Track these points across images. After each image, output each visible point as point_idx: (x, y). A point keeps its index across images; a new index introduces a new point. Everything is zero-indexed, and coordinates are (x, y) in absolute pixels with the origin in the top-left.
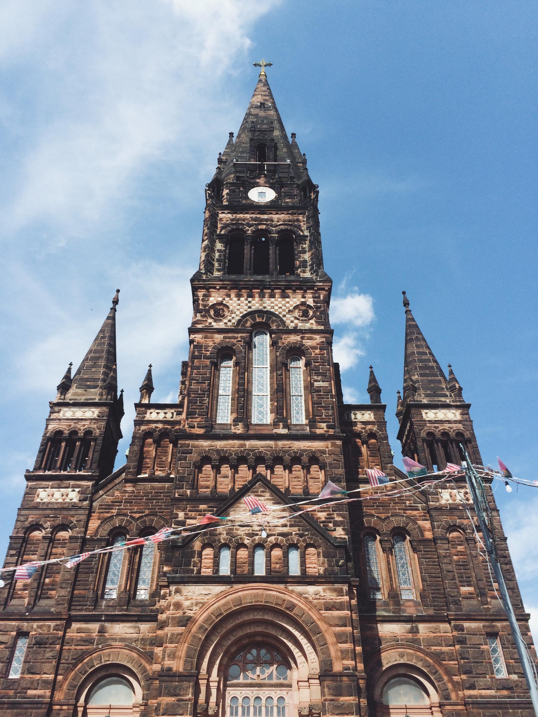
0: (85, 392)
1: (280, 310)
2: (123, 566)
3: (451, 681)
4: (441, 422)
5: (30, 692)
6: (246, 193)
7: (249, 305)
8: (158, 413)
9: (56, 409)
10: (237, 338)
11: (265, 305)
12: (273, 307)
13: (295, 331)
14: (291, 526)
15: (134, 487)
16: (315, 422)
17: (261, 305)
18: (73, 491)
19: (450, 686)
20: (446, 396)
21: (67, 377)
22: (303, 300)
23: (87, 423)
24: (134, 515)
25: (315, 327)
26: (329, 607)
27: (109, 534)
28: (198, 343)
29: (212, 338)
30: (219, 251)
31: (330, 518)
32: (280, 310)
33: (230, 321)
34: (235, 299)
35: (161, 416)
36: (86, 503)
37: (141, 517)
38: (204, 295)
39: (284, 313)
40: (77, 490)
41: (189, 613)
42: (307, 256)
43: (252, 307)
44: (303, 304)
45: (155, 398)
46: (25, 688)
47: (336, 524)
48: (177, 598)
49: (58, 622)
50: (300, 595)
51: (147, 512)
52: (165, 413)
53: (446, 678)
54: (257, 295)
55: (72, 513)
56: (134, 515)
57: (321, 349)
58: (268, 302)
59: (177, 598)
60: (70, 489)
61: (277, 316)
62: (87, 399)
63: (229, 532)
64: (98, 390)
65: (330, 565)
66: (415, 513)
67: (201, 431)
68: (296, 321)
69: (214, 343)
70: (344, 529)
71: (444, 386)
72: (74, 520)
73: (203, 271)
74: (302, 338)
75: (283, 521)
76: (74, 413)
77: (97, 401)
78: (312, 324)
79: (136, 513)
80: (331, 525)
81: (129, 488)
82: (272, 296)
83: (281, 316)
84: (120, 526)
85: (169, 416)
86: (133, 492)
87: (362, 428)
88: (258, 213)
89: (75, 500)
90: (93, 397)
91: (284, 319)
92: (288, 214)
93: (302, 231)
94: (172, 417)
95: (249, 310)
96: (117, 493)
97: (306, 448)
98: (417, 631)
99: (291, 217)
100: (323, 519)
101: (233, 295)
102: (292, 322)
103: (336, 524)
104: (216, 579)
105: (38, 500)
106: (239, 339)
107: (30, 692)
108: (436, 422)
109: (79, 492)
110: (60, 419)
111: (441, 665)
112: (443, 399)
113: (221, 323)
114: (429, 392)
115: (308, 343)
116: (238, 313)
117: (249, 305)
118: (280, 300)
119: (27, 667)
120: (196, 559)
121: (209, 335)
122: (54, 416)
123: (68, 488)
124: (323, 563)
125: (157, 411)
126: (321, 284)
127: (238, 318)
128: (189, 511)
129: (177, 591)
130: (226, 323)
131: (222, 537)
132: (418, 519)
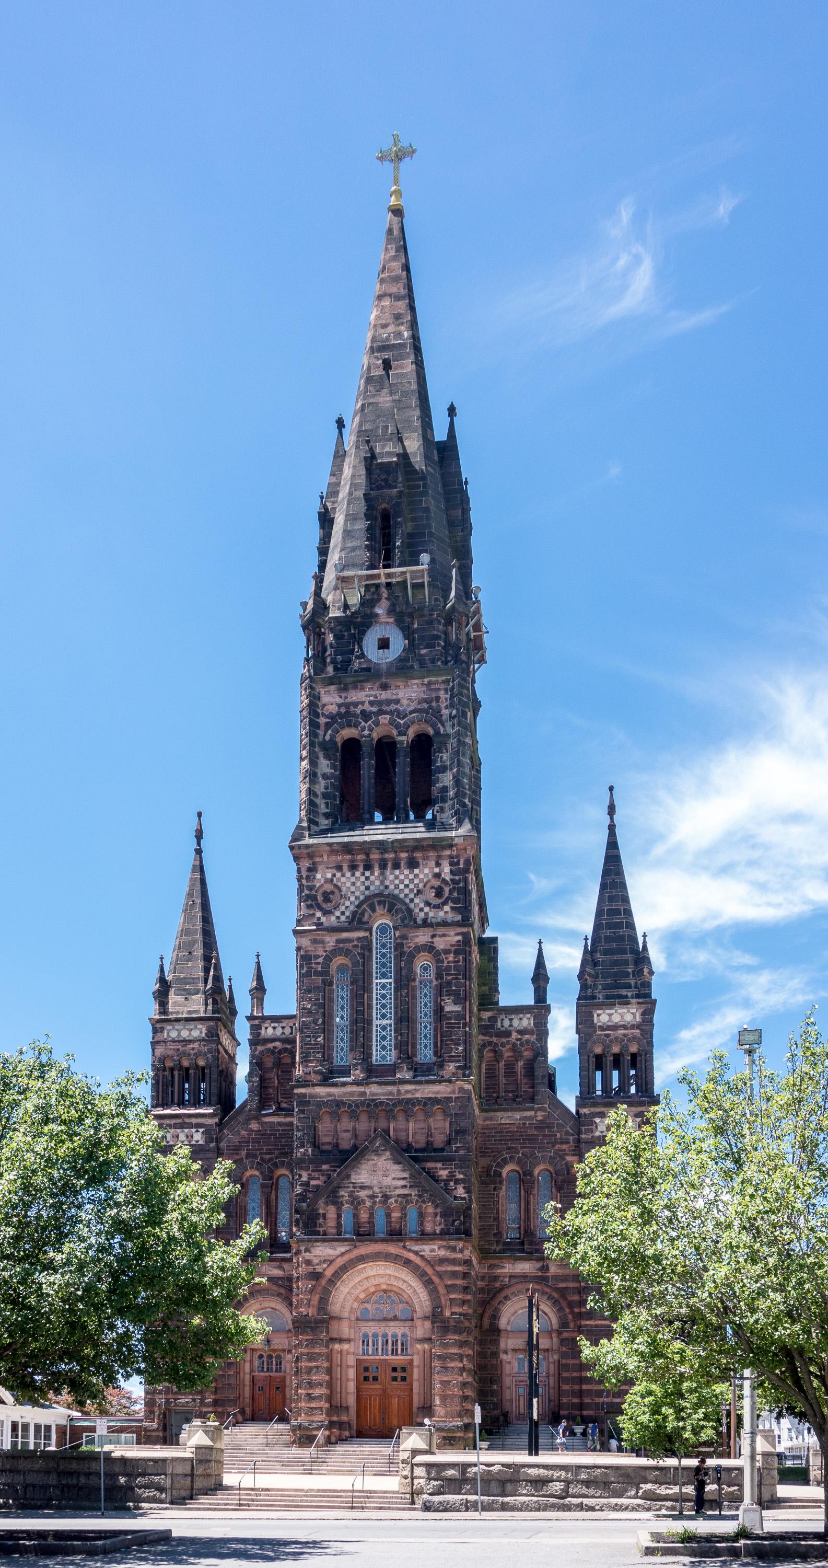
1: (407, 891)
2: (261, 1210)
3: (572, 1313)
4: (615, 1027)
7: (367, 883)
9: (158, 1025)
12: (397, 887)
13: (426, 923)
14: (411, 1186)
18: (197, 1131)
19: (570, 1317)
21: (162, 980)
23: (196, 1045)
24: (264, 1156)
26: (442, 1261)
28: (306, 951)
30: (325, 776)
31: (451, 1176)
32: (407, 891)
34: (348, 874)
36: (213, 1145)
37: (271, 1159)
39: (412, 896)
40: (201, 1130)
41: (319, 1269)
43: (372, 888)
45: (270, 1009)
47: (457, 1182)
48: (307, 1256)
50: (416, 1253)
53: (567, 1310)
56: (264, 1156)
57: (457, 953)
58: (392, 877)
59: (307, 1256)
60: (194, 1130)
61: (402, 902)
62: (189, 1012)
64: (200, 998)
65: (446, 1225)
66: (564, 1147)
68: (427, 909)
69: (326, 951)
70: (464, 1188)
71: (630, 970)
73: (305, 824)
75: (403, 1183)
76: (179, 1031)
77: (202, 1015)
78: (446, 912)
79: (266, 1154)
80: (452, 1183)
83: (407, 901)
87: (518, 1040)
91: (412, 906)
95: (367, 893)
97: (430, 1095)
98: (548, 1269)
100: (445, 1178)
102: (421, 910)
103: (457, 1182)
104: (338, 1237)
106: (355, 943)
108: (609, 1028)
110: (165, 1042)
111: (565, 1299)
113: (333, 918)
114: (609, 981)
116: (352, 899)
117: (367, 883)
118: (406, 872)
120: (321, 1220)
122: (159, 1037)
124: (440, 1224)
125: (273, 1025)
127: (352, 908)
128: (313, 1171)
129: (307, 1250)
130: (338, 918)
132: (567, 1155)
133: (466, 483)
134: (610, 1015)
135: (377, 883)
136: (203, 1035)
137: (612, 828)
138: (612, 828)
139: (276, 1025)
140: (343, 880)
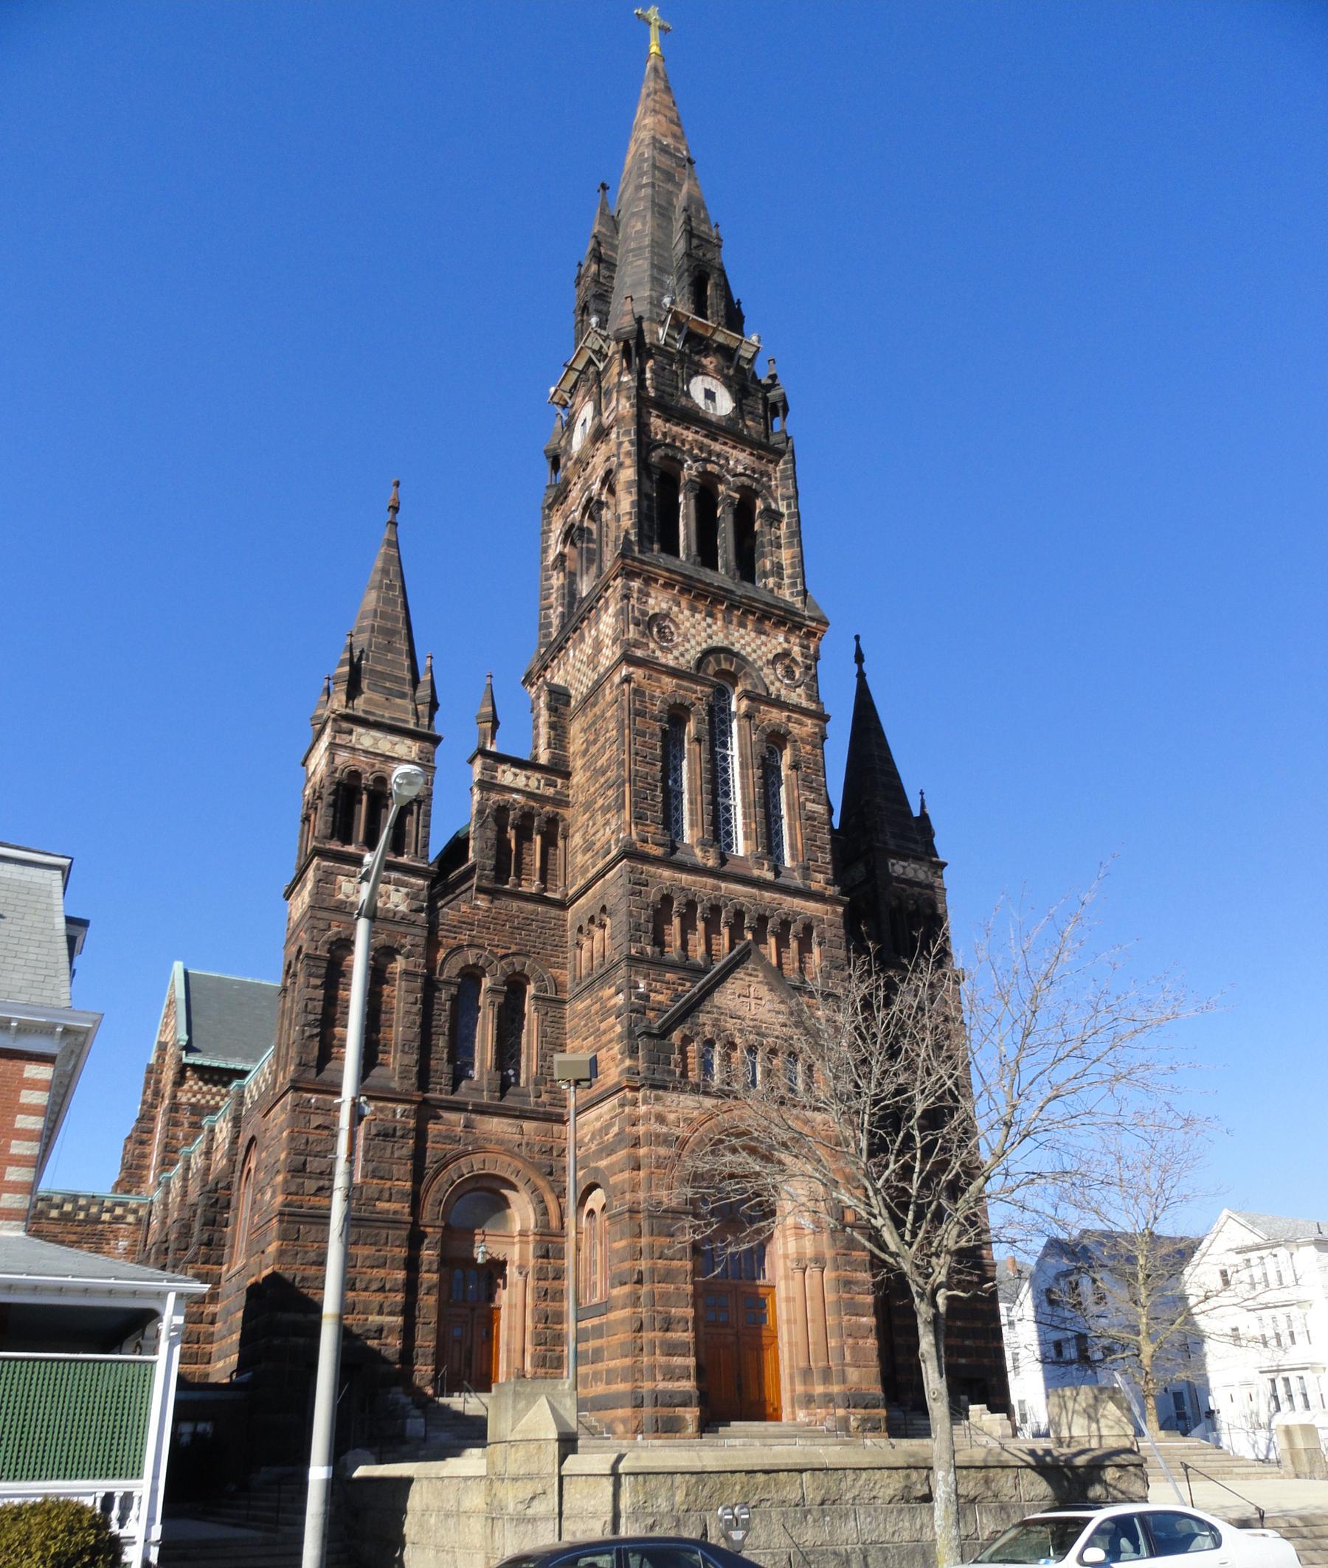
0: (387, 703)
5: (381, 1205)
6: (690, 377)
8: (516, 775)
9: (345, 725)
10: (695, 692)
11: (732, 639)
15: (492, 902)
16: (808, 868)
17: (726, 637)
20: (916, 842)
22: (786, 645)
25: (805, 704)
27: (458, 975)
29: (659, 681)
33: (682, 655)
35: (521, 782)
37: (506, 956)
38: (640, 591)
40: (404, 890)
42: (785, 556)
44: (786, 654)
46: (371, 1199)
49: (408, 1107)
51: (514, 948)
52: (528, 778)
54: (720, 616)
55: (402, 929)
60: (392, 887)
62: (393, 719)
63: (716, 1024)
67: (659, 851)
72: (407, 941)
74: (789, 718)
75: (782, 1019)
76: (376, 740)
81: (482, 902)
82: (742, 625)
84: (475, 965)
85: (533, 784)
86: (489, 910)
88: (706, 436)
89: (403, 908)
90: (403, 716)
92: (751, 454)
93: (776, 501)
94: (538, 788)
96: (464, 908)
99: (757, 465)
101: (684, 604)
105: (341, 897)
107: (381, 1205)
109: (407, 894)
110: (353, 749)
112: (913, 846)
113: (670, 657)
115: (795, 729)
119: (370, 1168)
121: (655, 674)
123: (389, 883)
126: (814, 624)
131: (707, 1028)
133: (739, 303)
134: (904, 867)
135: (721, 635)
136: (413, 755)
137: (861, 676)
138: (861, 676)
139: (518, 771)
140: (681, 616)
